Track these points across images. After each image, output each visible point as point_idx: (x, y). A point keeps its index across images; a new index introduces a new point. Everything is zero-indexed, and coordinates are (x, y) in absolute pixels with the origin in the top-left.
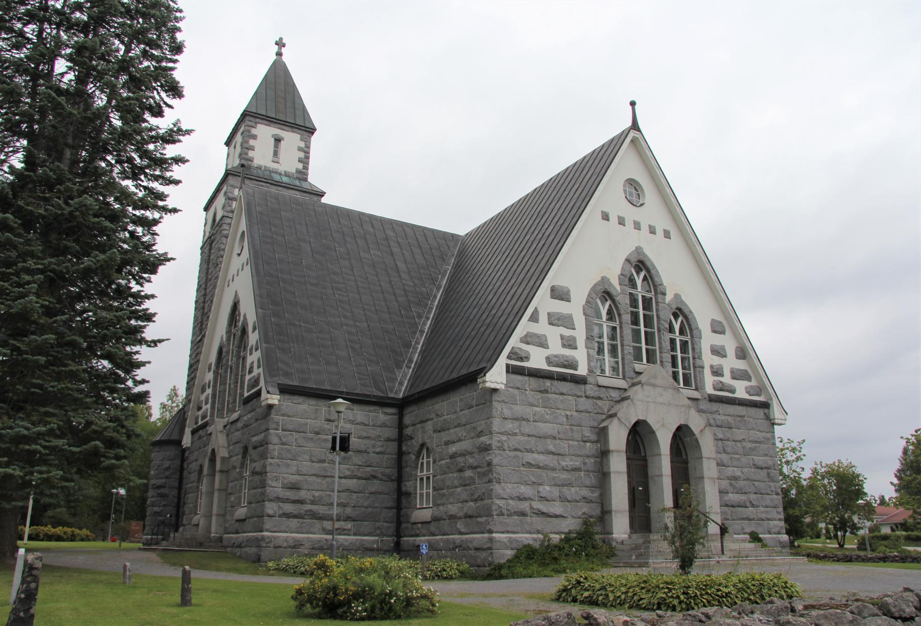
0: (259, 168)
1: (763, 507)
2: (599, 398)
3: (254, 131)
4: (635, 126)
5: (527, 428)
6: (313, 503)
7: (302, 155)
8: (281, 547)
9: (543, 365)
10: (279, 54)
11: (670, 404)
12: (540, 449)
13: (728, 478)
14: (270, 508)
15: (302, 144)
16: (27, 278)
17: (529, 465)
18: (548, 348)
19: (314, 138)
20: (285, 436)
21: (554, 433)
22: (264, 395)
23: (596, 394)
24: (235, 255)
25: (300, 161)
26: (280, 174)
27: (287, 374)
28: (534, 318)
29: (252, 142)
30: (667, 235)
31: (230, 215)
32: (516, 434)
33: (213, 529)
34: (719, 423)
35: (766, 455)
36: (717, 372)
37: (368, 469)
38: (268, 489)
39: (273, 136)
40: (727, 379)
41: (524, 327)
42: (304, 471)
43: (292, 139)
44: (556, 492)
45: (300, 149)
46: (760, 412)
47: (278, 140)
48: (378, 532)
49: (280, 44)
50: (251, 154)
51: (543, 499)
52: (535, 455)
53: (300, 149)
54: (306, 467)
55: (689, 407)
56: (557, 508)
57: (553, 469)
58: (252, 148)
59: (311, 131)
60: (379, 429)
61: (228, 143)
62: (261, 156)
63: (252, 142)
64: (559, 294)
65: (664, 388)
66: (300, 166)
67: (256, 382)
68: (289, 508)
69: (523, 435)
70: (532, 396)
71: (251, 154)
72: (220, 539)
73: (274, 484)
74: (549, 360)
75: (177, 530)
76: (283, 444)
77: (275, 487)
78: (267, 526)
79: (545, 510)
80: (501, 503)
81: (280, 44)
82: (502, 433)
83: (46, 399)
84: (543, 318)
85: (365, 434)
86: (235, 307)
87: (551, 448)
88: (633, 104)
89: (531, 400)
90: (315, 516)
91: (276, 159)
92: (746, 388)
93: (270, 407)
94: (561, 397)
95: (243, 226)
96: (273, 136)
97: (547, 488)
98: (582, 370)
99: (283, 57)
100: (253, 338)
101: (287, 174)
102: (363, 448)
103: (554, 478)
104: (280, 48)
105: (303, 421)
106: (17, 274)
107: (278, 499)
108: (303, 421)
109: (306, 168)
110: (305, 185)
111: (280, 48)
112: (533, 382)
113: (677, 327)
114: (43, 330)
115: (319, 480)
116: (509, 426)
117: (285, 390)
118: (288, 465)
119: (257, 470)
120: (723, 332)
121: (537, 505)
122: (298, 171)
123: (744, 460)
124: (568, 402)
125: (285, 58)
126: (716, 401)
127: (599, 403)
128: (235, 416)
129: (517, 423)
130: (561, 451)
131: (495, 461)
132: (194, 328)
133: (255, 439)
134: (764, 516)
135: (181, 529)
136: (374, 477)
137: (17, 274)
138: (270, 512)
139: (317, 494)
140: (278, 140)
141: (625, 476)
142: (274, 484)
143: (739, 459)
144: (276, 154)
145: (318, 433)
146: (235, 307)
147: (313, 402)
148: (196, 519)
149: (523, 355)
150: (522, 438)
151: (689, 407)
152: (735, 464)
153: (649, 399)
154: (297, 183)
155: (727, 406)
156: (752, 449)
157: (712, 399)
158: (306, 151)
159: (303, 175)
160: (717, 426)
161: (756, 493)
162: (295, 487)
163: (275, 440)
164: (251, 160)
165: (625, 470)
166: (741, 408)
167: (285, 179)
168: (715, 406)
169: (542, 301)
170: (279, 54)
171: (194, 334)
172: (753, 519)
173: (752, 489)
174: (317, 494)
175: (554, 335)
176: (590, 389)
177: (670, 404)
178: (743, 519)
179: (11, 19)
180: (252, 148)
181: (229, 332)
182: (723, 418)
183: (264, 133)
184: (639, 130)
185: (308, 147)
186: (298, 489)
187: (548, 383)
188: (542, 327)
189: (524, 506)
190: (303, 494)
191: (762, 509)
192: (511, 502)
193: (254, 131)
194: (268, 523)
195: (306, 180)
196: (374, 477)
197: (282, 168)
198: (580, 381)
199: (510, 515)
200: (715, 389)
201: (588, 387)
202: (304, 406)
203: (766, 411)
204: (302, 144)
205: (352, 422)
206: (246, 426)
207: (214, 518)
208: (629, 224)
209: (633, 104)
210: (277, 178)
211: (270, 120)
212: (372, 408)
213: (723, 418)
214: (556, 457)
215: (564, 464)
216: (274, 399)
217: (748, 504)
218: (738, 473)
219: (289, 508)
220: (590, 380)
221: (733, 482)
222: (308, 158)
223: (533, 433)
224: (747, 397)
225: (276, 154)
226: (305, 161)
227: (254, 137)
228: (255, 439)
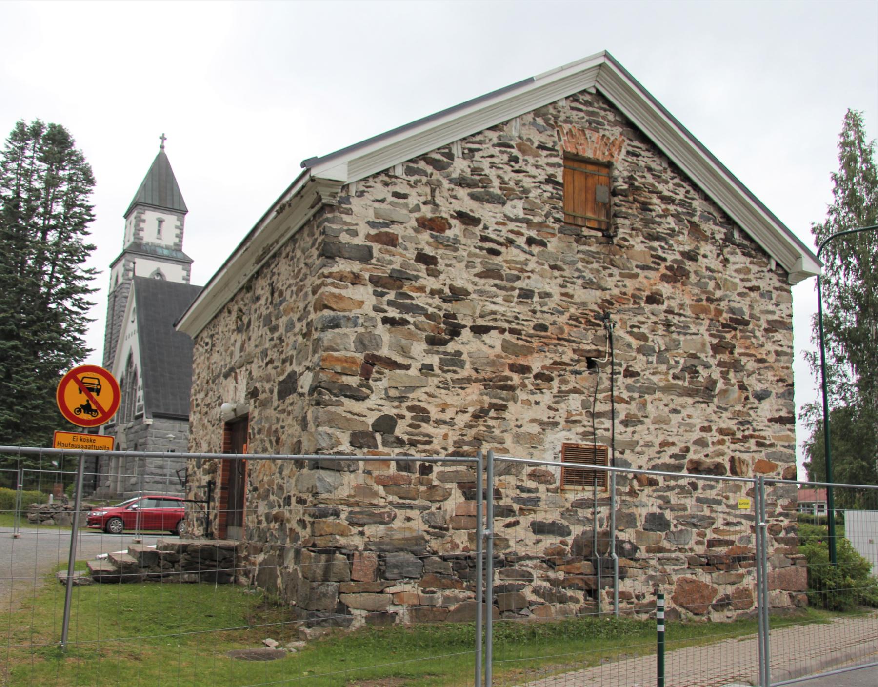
0: (147, 244)
3: (143, 217)
7: (178, 231)
8: (805, 671)
10: (162, 147)
15: (178, 223)
16: (28, 373)
19: (187, 217)
22: (144, 418)
24: (130, 322)
25: (177, 236)
26: (162, 248)
27: (158, 406)
29: (142, 225)
31: (128, 282)
33: (118, 489)
38: (147, 469)
39: (157, 219)
43: (171, 220)
45: (177, 227)
47: (161, 222)
50: (141, 234)
53: (177, 227)
58: (142, 230)
59: (184, 212)
61: (126, 216)
62: (149, 236)
63: (142, 225)
66: (177, 240)
67: (140, 409)
68: (158, 478)
71: (141, 234)
72: (122, 495)
75: (95, 490)
83: (39, 429)
86: (130, 356)
93: (148, 425)
95: (134, 305)
96: (157, 219)
100: (140, 381)
101: (167, 248)
106: (23, 371)
107: (152, 474)
109: (181, 241)
110: (179, 256)
114: (36, 397)
117: (156, 416)
119: (231, 379)
122: (175, 244)
125: (166, 151)
128: (131, 424)
132: (105, 354)
133: (140, 441)
135: (98, 489)
137: (23, 371)
138: (148, 480)
140: (161, 222)
144: (159, 232)
146: (130, 356)
147: (171, 421)
148: (108, 483)
154: (174, 254)
158: (181, 228)
159: (178, 247)
163: (151, 442)
164: (142, 239)
167: (166, 252)
170: (162, 147)
171: (104, 359)
180: (142, 230)
181: (127, 370)
183: (151, 217)
185: (182, 225)
193: (143, 217)
194: (147, 486)
195: (180, 251)
202: (166, 424)
204: (178, 223)
206: (136, 432)
207: (119, 483)
211: (155, 207)
216: (150, 421)
219: (158, 478)
222: (182, 233)
225: (159, 232)
226: (180, 236)
227: (144, 221)
228: (140, 441)
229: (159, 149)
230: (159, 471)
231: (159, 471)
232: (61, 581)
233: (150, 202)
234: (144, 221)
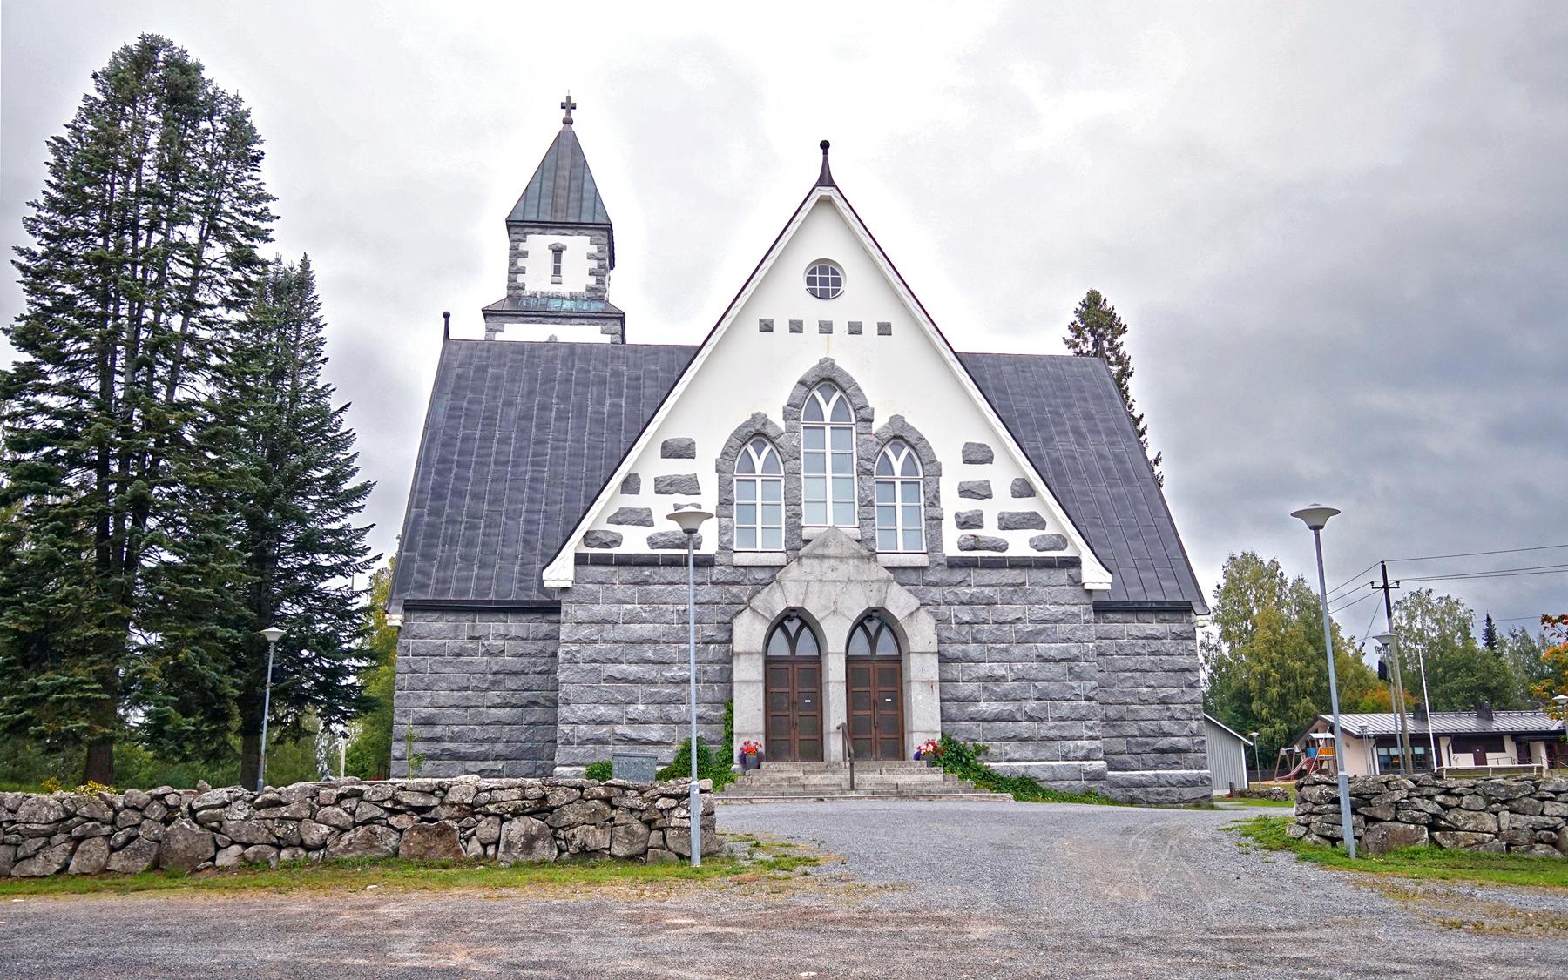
0: (534, 296)
1: (1053, 719)
2: (734, 583)
4: (826, 179)
5: (611, 632)
6: (452, 740)
9: (644, 549)
10: (568, 122)
11: (850, 581)
12: (631, 657)
13: (979, 679)
14: (397, 749)
17: (611, 679)
18: (652, 524)
20: (416, 662)
21: (653, 636)
23: (730, 578)
28: (631, 485)
29: (521, 263)
30: (885, 329)
32: (595, 641)
34: (965, 598)
35: (1069, 640)
36: (965, 522)
37: (526, 694)
38: (396, 728)
39: (550, 247)
40: (990, 530)
41: (610, 499)
42: (441, 701)
43: (579, 247)
44: (655, 711)
46: (1063, 576)
47: (558, 251)
48: (540, 772)
49: (569, 106)
50: (521, 279)
51: (633, 721)
52: (624, 666)
54: (443, 696)
55: (888, 581)
56: (655, 733)
57: (653, 683)
60: (541, 643)
62: (537, 280)
64: (679, 450)
65: (841, 558)
66: (592, 281)
69: (606, 641)
70: (620, 590)
73: (404, 720)
74: (652, 542)
76: (414, 672)
77: (403, 725)
78: (393, 772)
79: (634, 735)
80: (567, 729)
81: (569, 106)
82: (574, 642)
84: (647, 486)
85: (521, 651)
87: (650, 655)
88: (825, 145)
89: (620, 596)
90: (454, 756)
91: (556, 279)
92: (1031, 541)
94: (670, 588)
96: (550, 247)
97: (641, 707)
98: (709, 547)
99: (574, 127)
101: (574, 297)
102: (519, 668)
103: (652, 694)
104: (569, 113)
105: (439, 642)
107: (409, 739)
108: (439, 642)
111: (569, 113)
112: (626, 573)
113: (897, 466)
115: (460, 712)
116: (584, 632)
118: (420, 697)
120: (989, 460)
121: (619, 729)
122: (590, 289)
123: (1017, 650)
124: (687, 591)
125: (582, 129)
126: (961, 567)
127: (735, 589)
129: (597, 627)
130: (666, 658)
131: (561, 678)
134: (1053, 733)
136: (536, 704)
139: (457, 729)
140: (558, 251)
141: (761, 687)
142: (404, 720)
143: (1006, 650)
145: (459, 655)
147: (452, 617)
149: (609, 539)
150: (604, 646)
151: (888, 581)
152: (997, 657)
153: (810, 577)
155: (984, 571)
156: (1039, 633)
157: (953, 564)
159: (597, 293)
160: (962, 603)
161: (1039, 699)
162: (429, 722)
165: (761, 677)
166: (1016, 572)
167: (567, 305)
168: (959, 575)
169: (646, 460)
170: (568, 122)
172: (1030, 739)
173: (1034, 694)
174: (457, 729)
175: (661, 507)
176: (716, 573)
177: (850, 581)
178: (1009, 739)
179: (45, 256)
180: (522, 271)
182: (974, 590)
183: (538, 244)
184: (832, 184)
186: (434, 724)
187: (647, 572)
188: (646, 498)
189: (603, 731)
190: (438, 730)
191: (1051, 723)
192: (583, 727)
193: (523, 247)
196: (536, 704)
197: (565, 289)
198: (705, 562)
199: (581, 744)
200: (961, 548)
201: (716, 570)
202: (439, 624)
203: (1073, 571)
205: (505, 637)
208: (811, 328)
209: (825, 145)
210: (554, 305)
211: (544, 226)
212: (531, 617)
213: (974, 590)
214: (656, 667)
215: (668, 675)
217: (1018, 717)
218: (1000, 670)
219: (420, 748)
220: (719, 559)
221: (991, 685)
223: (622, 637)
224: (1034, 553)
226: (516, 254)
227: (525, 254)
229: (561, 126)
230: (425, 732)
231: (425, 732)
232: (1276, 700)
233: (533, 217)
234: (525, 254)
